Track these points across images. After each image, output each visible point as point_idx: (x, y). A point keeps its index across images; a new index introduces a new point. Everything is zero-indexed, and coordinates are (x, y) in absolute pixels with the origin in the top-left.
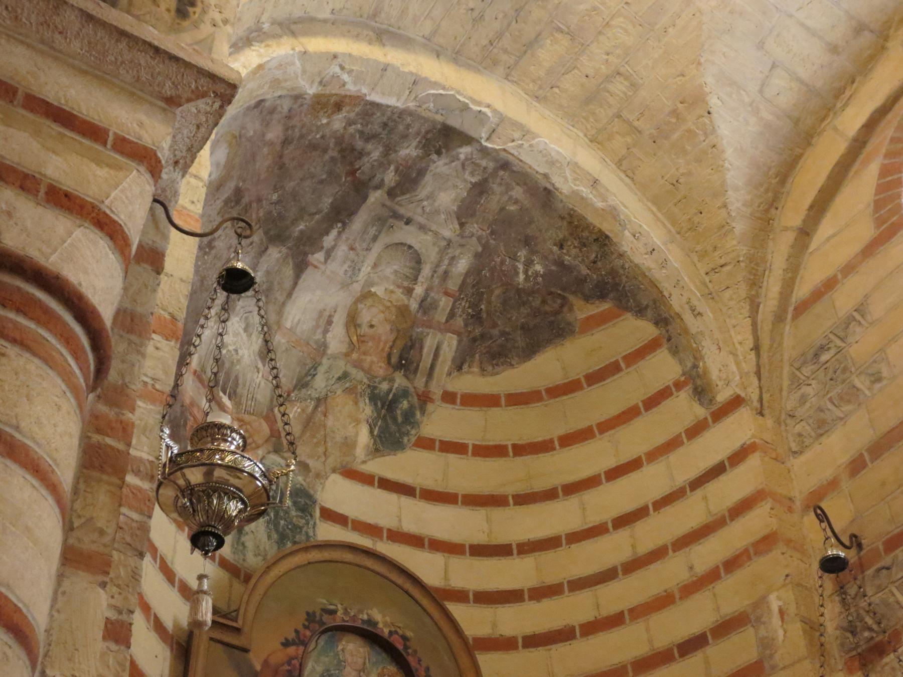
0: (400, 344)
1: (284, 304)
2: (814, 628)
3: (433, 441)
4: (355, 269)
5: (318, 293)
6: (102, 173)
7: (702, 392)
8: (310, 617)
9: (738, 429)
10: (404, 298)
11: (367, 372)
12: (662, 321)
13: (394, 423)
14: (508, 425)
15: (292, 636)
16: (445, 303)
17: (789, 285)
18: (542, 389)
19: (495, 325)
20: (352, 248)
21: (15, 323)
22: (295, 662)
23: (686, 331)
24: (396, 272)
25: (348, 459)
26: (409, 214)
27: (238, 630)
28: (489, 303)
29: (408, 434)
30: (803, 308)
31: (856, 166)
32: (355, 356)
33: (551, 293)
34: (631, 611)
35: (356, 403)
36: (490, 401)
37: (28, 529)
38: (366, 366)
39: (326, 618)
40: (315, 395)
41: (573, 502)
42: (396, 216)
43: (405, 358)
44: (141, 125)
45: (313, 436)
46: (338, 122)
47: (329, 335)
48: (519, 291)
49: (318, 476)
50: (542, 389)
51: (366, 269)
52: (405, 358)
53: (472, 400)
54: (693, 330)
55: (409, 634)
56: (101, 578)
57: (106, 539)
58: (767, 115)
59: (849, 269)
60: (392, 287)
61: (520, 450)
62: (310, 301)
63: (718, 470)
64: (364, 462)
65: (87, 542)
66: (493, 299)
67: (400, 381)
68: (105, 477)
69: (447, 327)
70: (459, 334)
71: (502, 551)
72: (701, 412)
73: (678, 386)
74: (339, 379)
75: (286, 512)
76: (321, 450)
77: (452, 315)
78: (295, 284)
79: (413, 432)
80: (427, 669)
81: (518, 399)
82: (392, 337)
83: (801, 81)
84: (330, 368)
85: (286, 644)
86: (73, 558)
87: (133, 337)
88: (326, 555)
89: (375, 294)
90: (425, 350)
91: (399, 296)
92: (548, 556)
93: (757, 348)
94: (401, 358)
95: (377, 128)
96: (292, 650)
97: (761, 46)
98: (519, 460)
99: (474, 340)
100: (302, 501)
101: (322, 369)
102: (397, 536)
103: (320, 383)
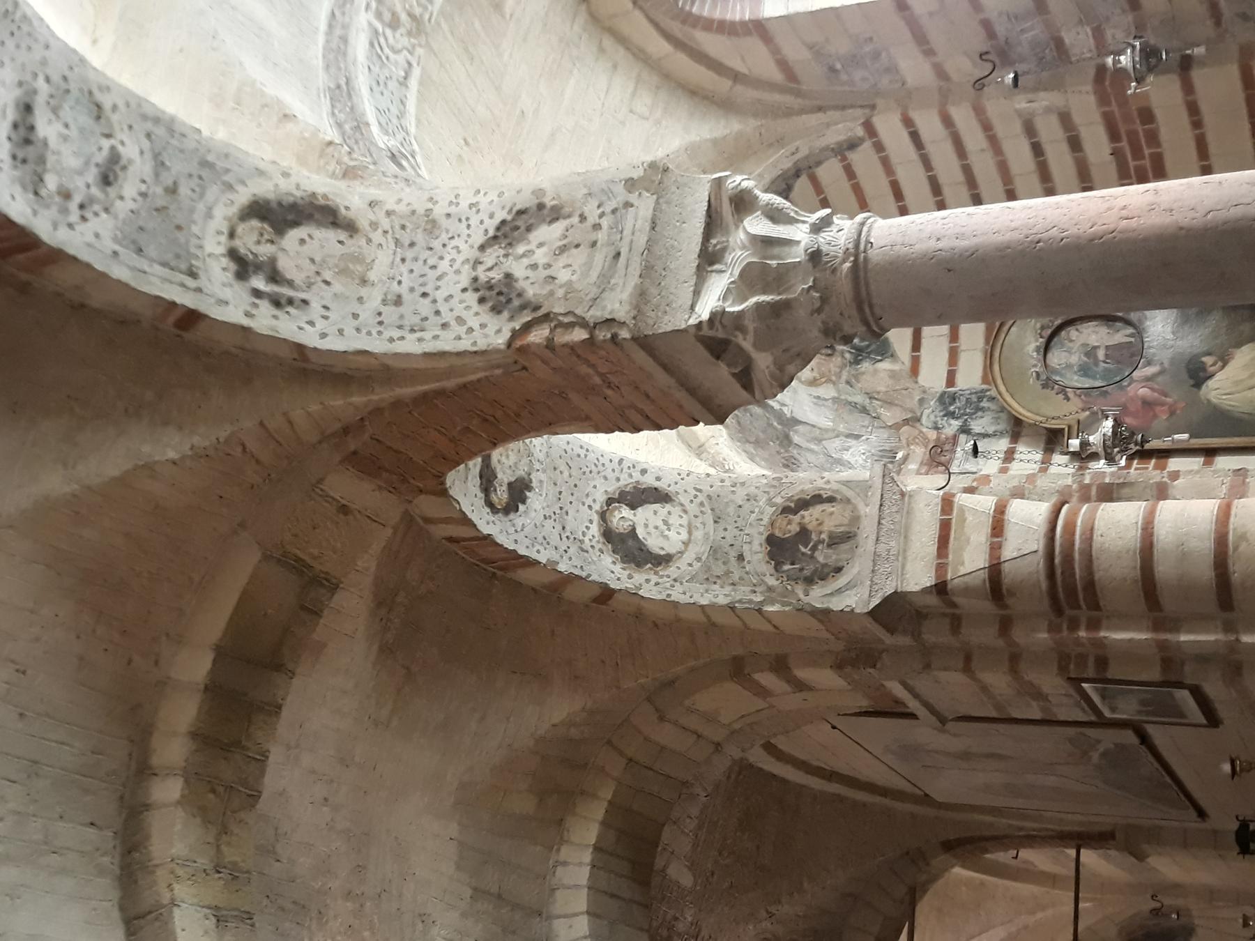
7: (853, 145)
8: (1045, 386)
9: (890, 127)
12: (797, 174)
15: (1061, 396)
17: (772, 86)
23: (807, 157)
32: (834, 378)
35: (863, 373)
49: (924, 392)
54: (807, 152)
58: (658, 114)
59: (775, 51)
63: (915, 137)
72: (867, 145)
73: (844, 159)
83: (636, 89)
85: (1068, 399)
96: (1071, 395)
101: (850, 399)
103: (859, 399)
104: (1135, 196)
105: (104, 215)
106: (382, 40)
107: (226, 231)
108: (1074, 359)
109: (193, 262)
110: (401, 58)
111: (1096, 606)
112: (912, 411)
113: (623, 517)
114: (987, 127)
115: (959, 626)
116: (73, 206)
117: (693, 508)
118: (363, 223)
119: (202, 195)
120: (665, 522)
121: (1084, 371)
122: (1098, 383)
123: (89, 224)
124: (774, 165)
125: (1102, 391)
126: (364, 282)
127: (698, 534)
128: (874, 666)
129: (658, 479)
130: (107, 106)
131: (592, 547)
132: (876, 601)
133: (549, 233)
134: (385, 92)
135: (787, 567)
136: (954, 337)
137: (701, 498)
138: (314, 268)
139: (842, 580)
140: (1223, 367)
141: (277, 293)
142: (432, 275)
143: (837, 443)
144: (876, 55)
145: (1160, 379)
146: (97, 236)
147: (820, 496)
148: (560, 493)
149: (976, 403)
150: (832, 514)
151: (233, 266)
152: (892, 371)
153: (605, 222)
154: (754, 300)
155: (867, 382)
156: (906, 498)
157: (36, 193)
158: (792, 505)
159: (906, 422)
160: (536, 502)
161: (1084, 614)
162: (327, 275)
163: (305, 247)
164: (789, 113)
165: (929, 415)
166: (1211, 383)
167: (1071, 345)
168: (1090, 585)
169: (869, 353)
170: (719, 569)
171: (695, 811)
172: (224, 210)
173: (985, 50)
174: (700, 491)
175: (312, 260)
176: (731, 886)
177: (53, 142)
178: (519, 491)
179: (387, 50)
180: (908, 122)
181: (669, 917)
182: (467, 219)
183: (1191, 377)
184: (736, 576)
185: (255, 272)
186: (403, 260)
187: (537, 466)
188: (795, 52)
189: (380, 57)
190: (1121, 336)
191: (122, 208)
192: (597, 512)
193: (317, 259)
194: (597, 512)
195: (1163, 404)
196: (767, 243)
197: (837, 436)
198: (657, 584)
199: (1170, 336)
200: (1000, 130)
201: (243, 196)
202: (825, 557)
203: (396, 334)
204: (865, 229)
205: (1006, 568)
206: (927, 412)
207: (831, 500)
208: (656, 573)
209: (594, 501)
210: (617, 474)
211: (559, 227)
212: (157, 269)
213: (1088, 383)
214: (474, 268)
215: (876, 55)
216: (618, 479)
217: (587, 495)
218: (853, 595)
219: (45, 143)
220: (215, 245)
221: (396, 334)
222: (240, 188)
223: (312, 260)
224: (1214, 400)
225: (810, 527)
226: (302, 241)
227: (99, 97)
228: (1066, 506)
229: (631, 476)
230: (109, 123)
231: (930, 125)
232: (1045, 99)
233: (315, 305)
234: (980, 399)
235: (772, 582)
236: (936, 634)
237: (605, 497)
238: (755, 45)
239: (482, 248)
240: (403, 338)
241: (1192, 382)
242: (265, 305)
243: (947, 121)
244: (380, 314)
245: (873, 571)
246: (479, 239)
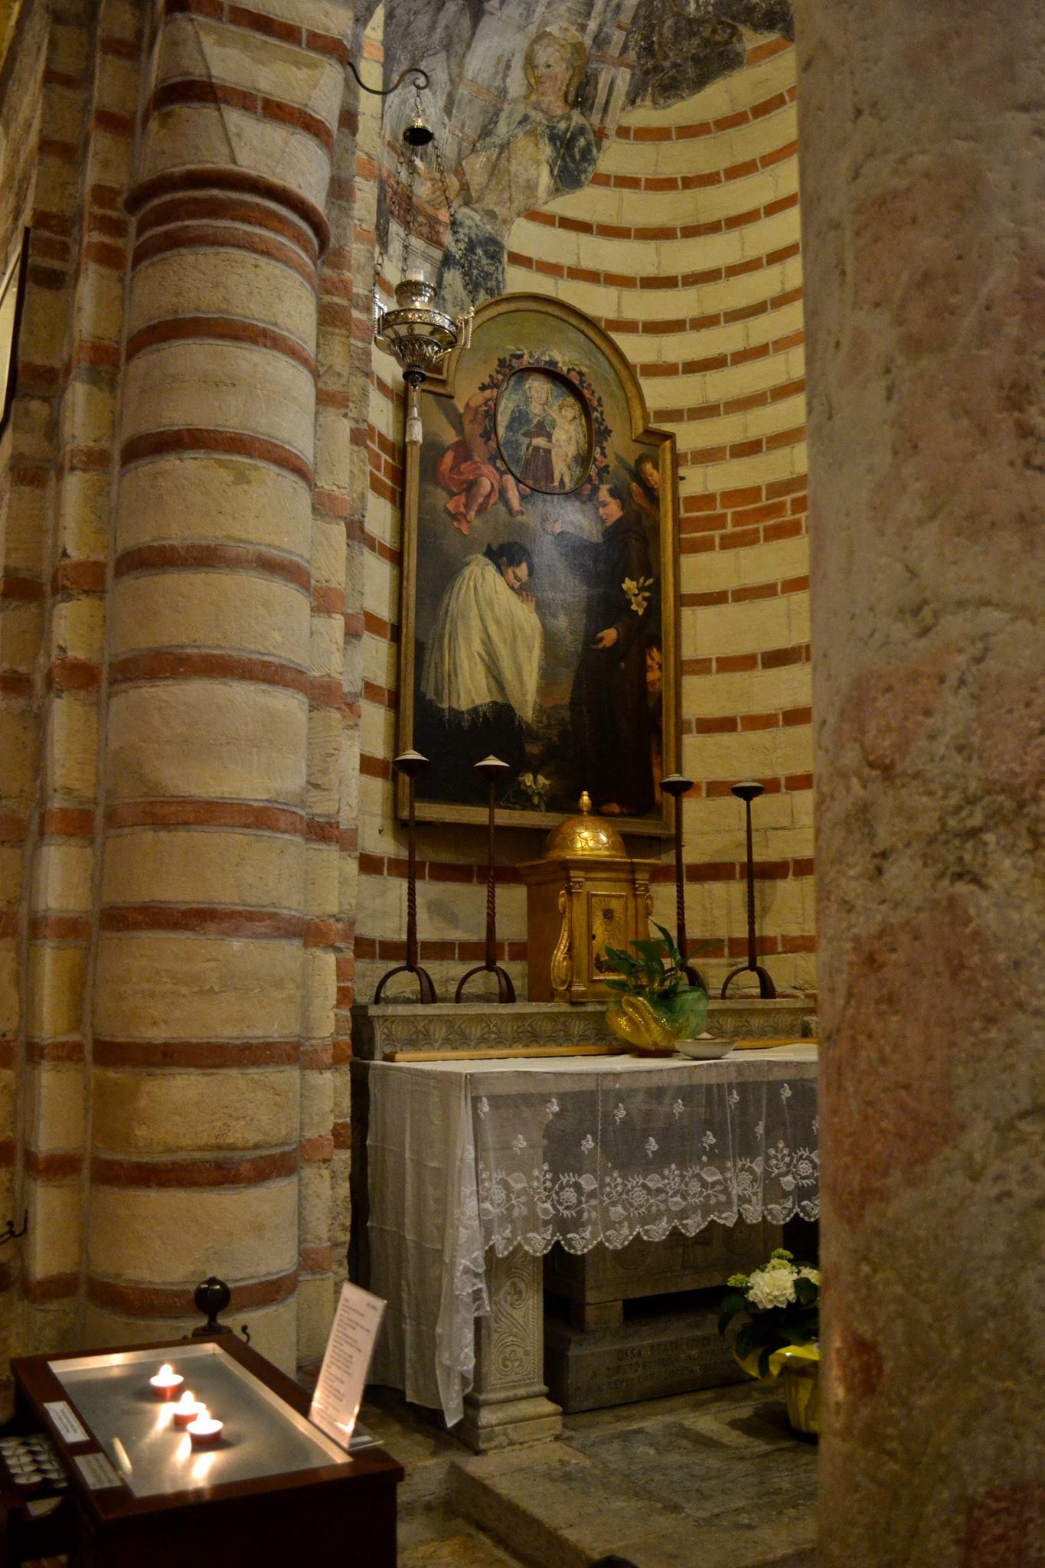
0: (576, 82)
1: (464, 56)
3: (608, 177)
5: (496, 39)
6: (302, 74)
8: (502, 363)
10: (578, 34)
11: (545, 112)
13: (572, 162)
14: (680, 157)
15: (487, 380)
16: (618, 37)
18: (711, 121)
19: (666, 57)
21: (260, 236)
22: (491, 403)
24: (569, 9)
25: (531, 201)
27: (443, 382)
28: (661, 35)
29: (585, 171)
32: (533, 98)
33: (722, 23)
34: (775, 343)
36: (660, 134)
37: (295, 399)
38: (544, 106)
39: (515, 363)
40: (498, 142)
41: (734, 235)
43: (581, 96)
44: (327, 14)
45: (498, 184)
47: (508, 80)
48: (690, 22)
49: (505, 222)
50: (711, 121)
52: (581, 96)
53: (645, 134)
55: (584, 370)
56: (343, 411)
57: (343, 381)
60: (566, 25)
61: (688, 183)
62: (489, 49)
64: (545, 203)
65: (333, 385)
66: (665, 31)
67: (577, 118)
68: (337, 331)
69: (620, 62)
70: (631, 67)
71: (668, 283)
74: (520, 123)
75: (478, 261)
76: (506, 196)
77: (625, 48)
78: (473, 34)
79: (590, 169)
80: (600, 399)
81: (688, 132)
82: (568, 76)
84: (511, 113)
85: (483, 388)
86: (324, 399)
87: (343, 203)
88: (513, 306)
89: (550, 34)
90: (600, 86)
91: (574, 33)
92: (708, 288)
94: (577, 96)
96: (488, 393)
98: (688, 192)
99: (646, 73)
100: (492, 249)
101: (503, 115)
102: (577, 274)
103: (502, 129)
104: (465, 1287)
108: (535, 409)
112: (479, 200)
115: (118, 52)
121: (519, 419)
122: (501, 431)
125: (489, 433)
140: (512, 588)
145: (503, 509)
152: (537, 186)
155: (524, 147)
159: (465, 187)
161: (129, 244)
166: (491, 570)
167: (556, 408)
168: (175, 242)
169: (563, 158)
183: (502, 547)
190: (562, 468)
195: (467, 507)
197: (452, 81)
199: (558, 529)
205: (209, 112)
206: (477, 217)
213: (503, 420)
224: (467, 572)
234: (490, 292)
241: (495, 547)
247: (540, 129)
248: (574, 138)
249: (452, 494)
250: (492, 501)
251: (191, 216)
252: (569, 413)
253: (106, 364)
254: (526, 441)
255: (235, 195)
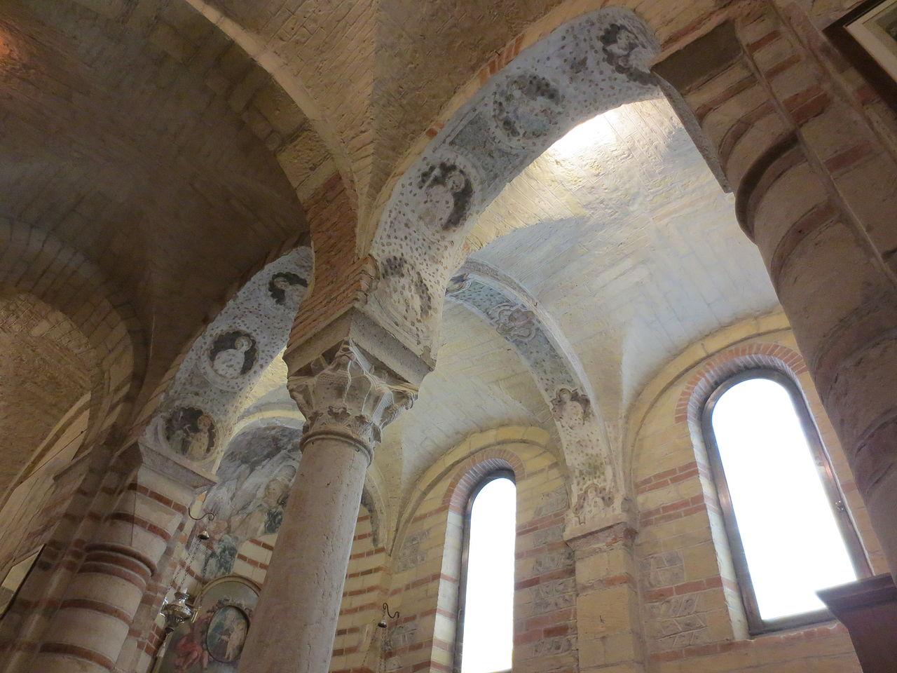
1: (243, 482)
2: (374, 640)
4: (272, 472)
6: (167, 517)
7: (375, 541)
8: (220, 602)
9: (378, 560)
12: (370, 511)
17: (414, 510)
20: (272, 465)
26: (294, 457)
30: (417, 519)
31: (445, 477)
42: (290, 457)
46: (273, 432)
49: (241, 542)
51: (276, 472)
59: (431, 514)
63: (369, 572)
67: (280, 509)
73: (370, 535)
75: (225, 556)
76: (245, 531)
85: (208, 612)
88: (232, 579)
93: (397, 530)
95: (286, 433)
97: (423, 432)
103: (251, 508)
104: (337, 603)
105: (492, 114)
106: (508, 308)
107: (464, 170)
109: (457, 147)
110: (496, 315)
111: (83, 570)
113: (244, 346)
114: (362, 608)
116: (502, 100)
117: (233, 383)
118: (445, 234)
119: (484, 168)
120: (232, 366)
121: (219, 626)
122: (209, 631)
123: (492, 103)
124: (379, 500)
126: (420, 218)
127: (218, 379)
128: (105, 443)
129: (255, 372)
130: (536, 141)
131: (235, 323)
132: (142, 448)
133: (417, 303)
134: (486, 297)
135: (182, 413)
136: (263, 566)
137: (237, 389)
138: (434, 200)
139: (161, 437)
141: (430, 177)
142: (414, 247)
143: (233, 487)
144: (414, 561)
146: (486, 105)
147: (213, 446)
148: (269, 318)
149: (224, 565)
150: (200, 447)
151: (448, 164)
152: (258, 530)
153: (414, 328)
154: (350, 378)
156: (193, 489)
157: (515, 82)
158: (213, 431)
159: (229, 527)
160: (269, 303)
161: (81, 563)
162: (429, 204)
163: (444, 202)
164: (401, 514)
165: (228, 539)
168: (98, 570)
170: (196, 381)
171: (70, 345)
172: (475, 176)
173: (400, 615)
174: (240, 390)
175: (438, 202)
176: (22, 360)
177: (532, 103)
178: (278, 295)
179: (503, 308)
180: (377, 570)
181: (20, 313)
182: (433, 276)
184: (188, 387)
185: (442, 173)
186: (424, 240)
187: (287, 311)
188: (427, 523)
189: (501, 303)
191: (492, 125)
192: (251, 333)
193: (437, 205)
194: (251, 333)
196: (377, 400)
197: (236, 489)
198: (202, 347)
200: (357, 615)
201: (476, 187)
202: (178, 435)
203: (393, 215)
204: (366, 452)
205: (129, 526)
207: (208, 450)
208: (207, 349)
209: (257, 334)
210: (266, 352)
211: (418, 309)
212: (461, 127)
213: (212, 626)
214: (411, 265)
215: (414, 561)
216: (263, 352)
217: (261, 332)
218: (150, 438)
219: (534, 99)
220: (460, 161)
221: (393, 215)
222: (479, 187)
223: (438, 202)
225: (198, 434)
226: (447, 202)
227: (542, 138)
228: (150, 574)
229: (262, 359)
230: (529, 138)
231: (373, 580)
232: (366, 641)
233: (418, 191)
234: (226, 569)
235: (177, 403)
236: (110, 479)
237: (257, 341)
238: (438, 504)
239: (419, 274)
240: (390, 216)
242: (426, 169)
243: (371, 589)
244: (404, 215)
245: (159, 454)
246: (423, 275)
247: (265, 510)
248: (277, 515)
249: (179, 657)
250: (195, 663)
251: (106, 561)
252: (241, 627)
253: (54, 607)
254: (219, 636)
255: (127, 557)
